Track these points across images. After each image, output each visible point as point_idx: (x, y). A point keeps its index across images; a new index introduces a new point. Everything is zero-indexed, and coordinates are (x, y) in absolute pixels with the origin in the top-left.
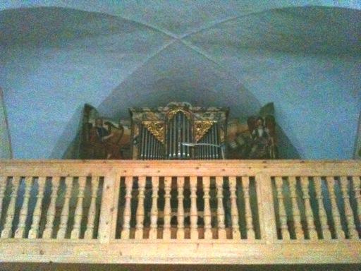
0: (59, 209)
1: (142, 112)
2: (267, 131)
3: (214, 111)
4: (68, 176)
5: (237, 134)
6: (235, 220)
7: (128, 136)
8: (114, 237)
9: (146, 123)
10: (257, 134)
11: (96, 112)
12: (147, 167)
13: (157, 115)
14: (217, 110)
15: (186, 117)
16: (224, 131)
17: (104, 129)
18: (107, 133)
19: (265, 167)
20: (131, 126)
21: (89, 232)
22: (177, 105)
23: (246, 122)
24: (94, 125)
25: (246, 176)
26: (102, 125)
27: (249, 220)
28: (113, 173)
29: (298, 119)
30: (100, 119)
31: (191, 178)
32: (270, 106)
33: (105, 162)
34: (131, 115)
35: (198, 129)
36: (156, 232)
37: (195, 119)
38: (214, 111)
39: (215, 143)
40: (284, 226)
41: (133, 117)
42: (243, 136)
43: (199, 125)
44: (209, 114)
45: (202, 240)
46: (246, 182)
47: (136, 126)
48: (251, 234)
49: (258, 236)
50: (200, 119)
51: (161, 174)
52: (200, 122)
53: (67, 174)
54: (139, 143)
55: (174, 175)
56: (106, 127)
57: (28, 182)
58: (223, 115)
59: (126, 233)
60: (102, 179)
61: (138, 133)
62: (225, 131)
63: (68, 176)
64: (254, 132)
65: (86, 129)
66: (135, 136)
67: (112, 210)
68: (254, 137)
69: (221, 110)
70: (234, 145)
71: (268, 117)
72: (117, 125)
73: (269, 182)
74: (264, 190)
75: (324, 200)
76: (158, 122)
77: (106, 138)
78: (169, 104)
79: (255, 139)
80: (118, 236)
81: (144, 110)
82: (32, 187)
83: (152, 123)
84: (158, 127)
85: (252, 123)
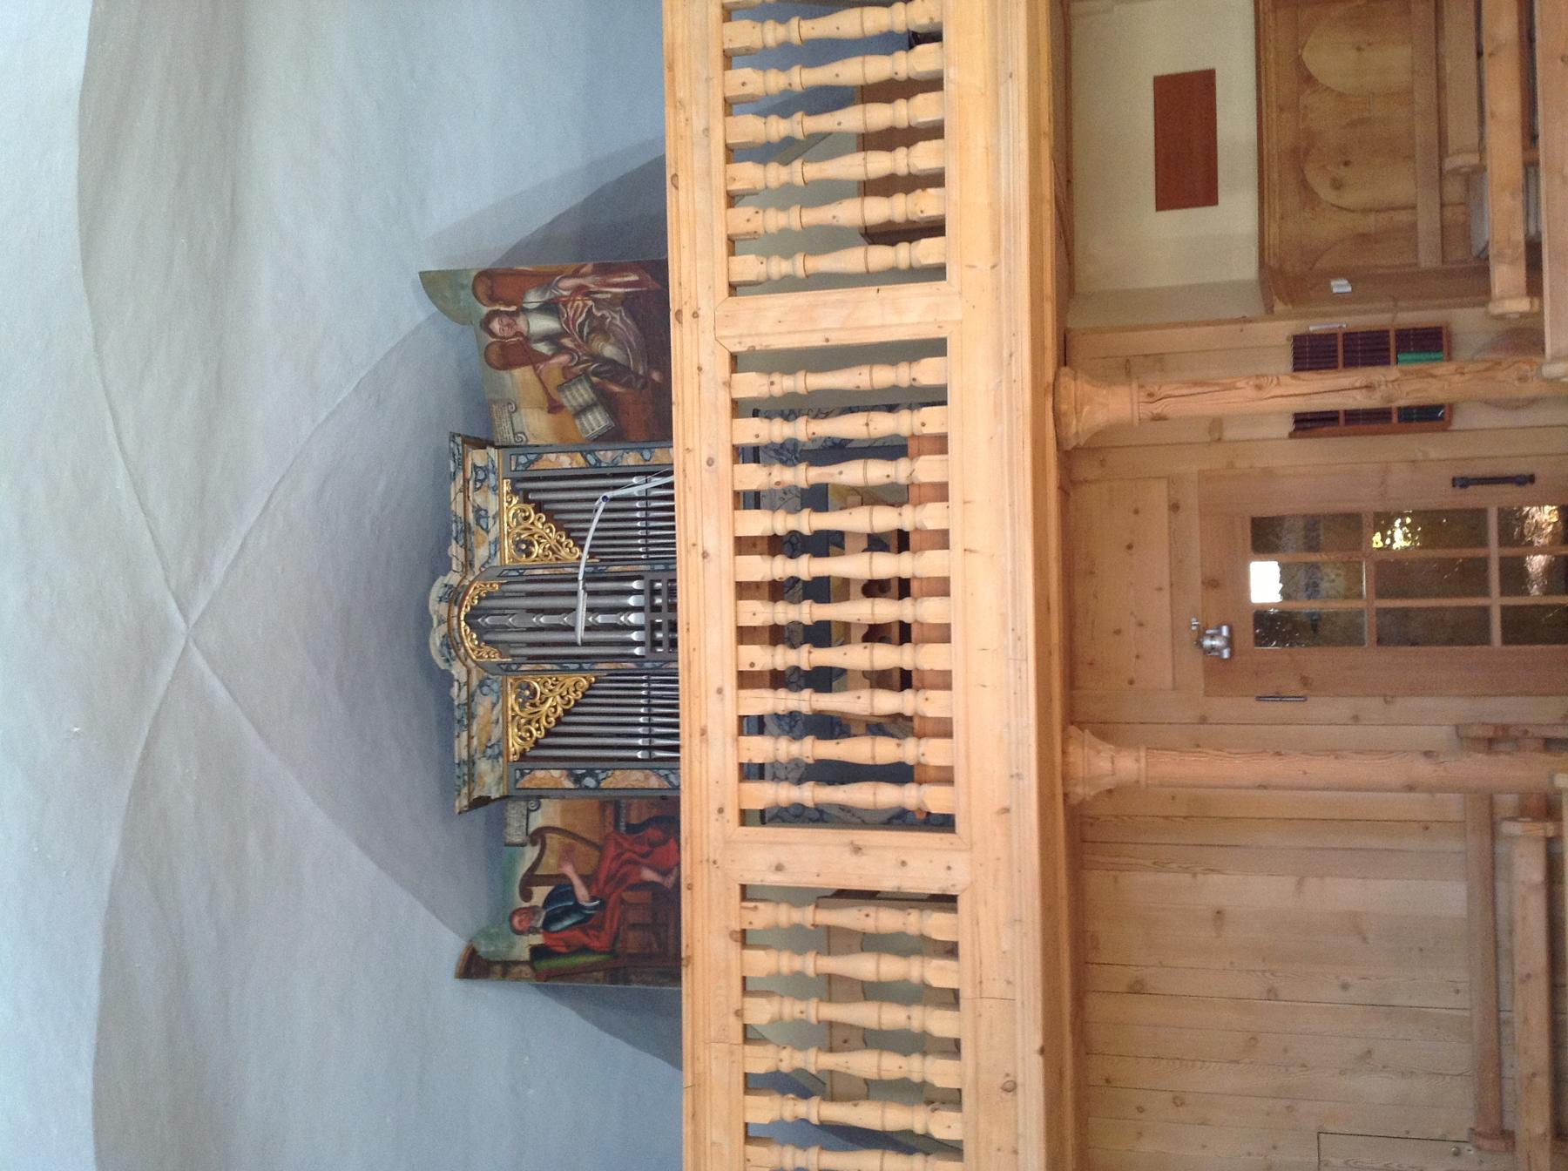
0: (839, 451)
1: (471, 762)
2: (533, 299)
3: (465, 490)
4: (739, 1013)
5: (554, 407)
6: (883, 425)
7: (564, 811)
8: (949, 836)
9: (515, 744)
10: (548, 338)
11: (485, 934)
12: (703, 732)
13: (483, 706)
14: (460, 481)
15: (490, 596)
16: (539, 456)
17: (549, 900)
18: (562, 890)
19: (695, 315)
20: (527, 798)
21: (936, 924)
22: (444, 628)
23: (505, 374)
24: (537, 939)
25: (728, 385)
26: (533, 910)
27: (884, 376)
28: (727, 857)
29: (495, 173)
30: (516, 922)
31: (736, 442)
32: (433, 283)
33: (690, 887)
34: (483, 801)
35: (537, 550)
36: (931, 694)
37: (496, 562)
38: (465, 490)
39: (587, 530)
40: (902, 254)
41: (494, 795)
42: (560, 388)
43: (523, 546)
44: (477, 510)
45: (953, 538)
46: (752, 385)
47: (525, 782)
48: (927, 372)
49: (937, 347)
50: (497, 542)
51: (730, 681)
52: (507, 543)
53: (732, 1020)
54: (593, 766)
55: (730, 635)
56: (540, 894)
57: (761, 1012)
58: (477, 457)
59: (933, 798)
60: (745, 892)
61: (556, 773)
62: (540, 451)
63: (739, 1013)
64: (543, 348)
65: (549, 969)
66: (569, 784)
67: (857, 850)
68: (560, 350)
69: (461, 464)
70: (597, 421)
71: (484, 295)
72: (531, 853)
73: (748, 304)
74: (783, 322)
75: (812, 112)
76: (511, 699)
77: (582, 893)
78: (440, 662)
79: (567, 342)
80: (944, 823)
81: (465, 755)
82: (779, 950)
83: (505, 721)
84: (530, 698)
85: (514, 353)
